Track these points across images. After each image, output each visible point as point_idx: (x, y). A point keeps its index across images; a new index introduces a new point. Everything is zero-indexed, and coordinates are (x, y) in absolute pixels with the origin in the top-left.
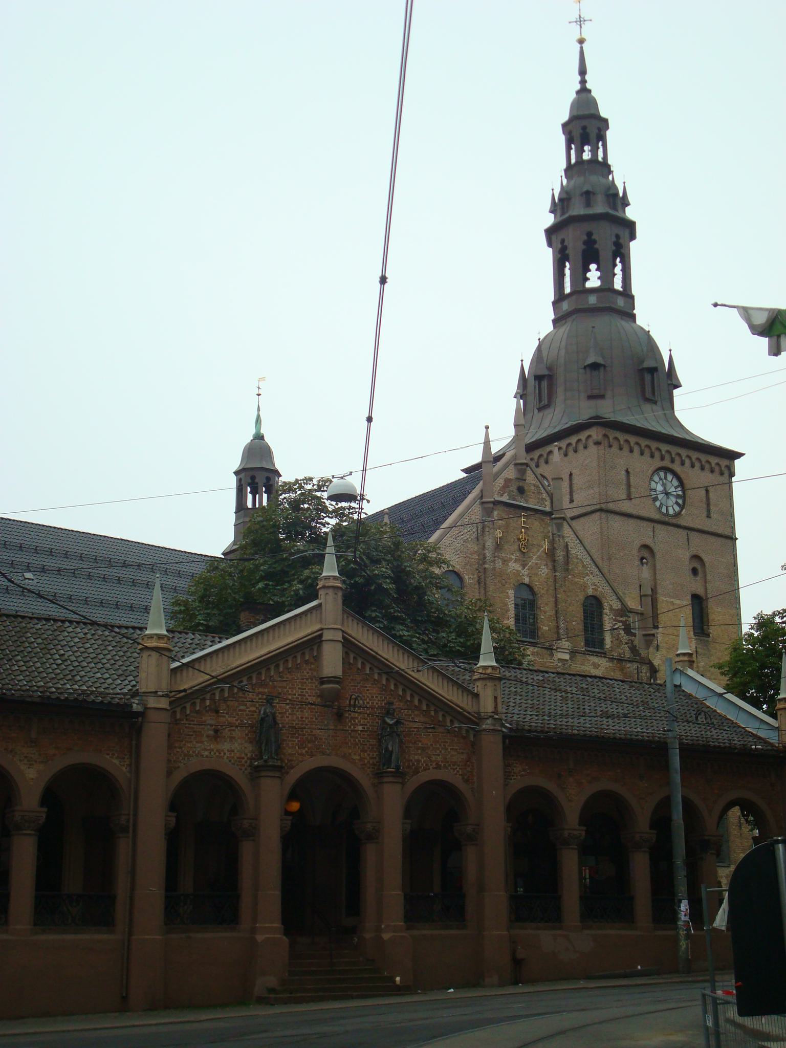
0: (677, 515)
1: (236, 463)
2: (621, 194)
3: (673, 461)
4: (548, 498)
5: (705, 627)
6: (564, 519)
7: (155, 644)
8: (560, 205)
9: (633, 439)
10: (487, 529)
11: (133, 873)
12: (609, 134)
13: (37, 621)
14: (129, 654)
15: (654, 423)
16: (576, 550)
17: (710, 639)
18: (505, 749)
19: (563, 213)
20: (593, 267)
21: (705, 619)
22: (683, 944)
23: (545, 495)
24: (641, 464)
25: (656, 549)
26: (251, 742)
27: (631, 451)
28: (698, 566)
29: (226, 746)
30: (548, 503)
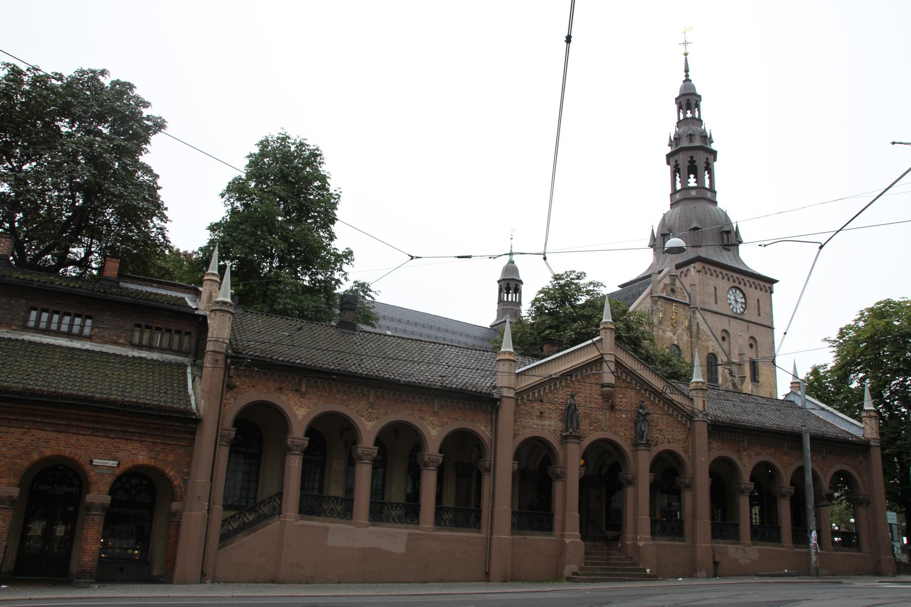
0: (742, 313)
1: (498, 276)
2: (709, 136)
3: (740, 283)
4: (687, 296)
5: (756, 377)
6: (696, 308)
7: (507, 357)
8: (675, 141)
9: (718, 270)
10: (654, 312)
11: (493, 496)
12: (702, 104)
13: (429, 344)
14: (484, 365)
15: (730, 263)
16: (703, 327)
17: (759, 384)
18: (709, 433)
19: (676, 145)
20: (692, 176)
21: (756, 373)
22: (814, 558)
23: (686, 294)
24: (723, 284)
25: (730, 332)
26: (561, 421)
27: (717, 277)
28: (753, 343)
29: (547, 422)
30: (688, 299)
